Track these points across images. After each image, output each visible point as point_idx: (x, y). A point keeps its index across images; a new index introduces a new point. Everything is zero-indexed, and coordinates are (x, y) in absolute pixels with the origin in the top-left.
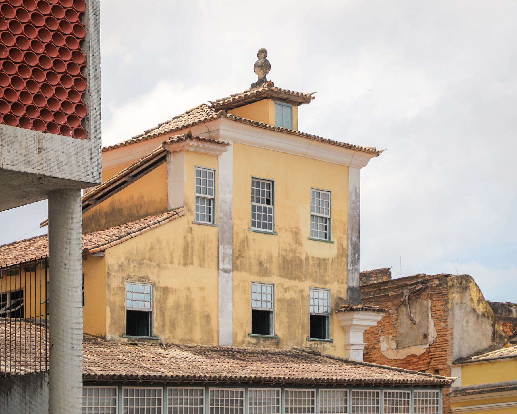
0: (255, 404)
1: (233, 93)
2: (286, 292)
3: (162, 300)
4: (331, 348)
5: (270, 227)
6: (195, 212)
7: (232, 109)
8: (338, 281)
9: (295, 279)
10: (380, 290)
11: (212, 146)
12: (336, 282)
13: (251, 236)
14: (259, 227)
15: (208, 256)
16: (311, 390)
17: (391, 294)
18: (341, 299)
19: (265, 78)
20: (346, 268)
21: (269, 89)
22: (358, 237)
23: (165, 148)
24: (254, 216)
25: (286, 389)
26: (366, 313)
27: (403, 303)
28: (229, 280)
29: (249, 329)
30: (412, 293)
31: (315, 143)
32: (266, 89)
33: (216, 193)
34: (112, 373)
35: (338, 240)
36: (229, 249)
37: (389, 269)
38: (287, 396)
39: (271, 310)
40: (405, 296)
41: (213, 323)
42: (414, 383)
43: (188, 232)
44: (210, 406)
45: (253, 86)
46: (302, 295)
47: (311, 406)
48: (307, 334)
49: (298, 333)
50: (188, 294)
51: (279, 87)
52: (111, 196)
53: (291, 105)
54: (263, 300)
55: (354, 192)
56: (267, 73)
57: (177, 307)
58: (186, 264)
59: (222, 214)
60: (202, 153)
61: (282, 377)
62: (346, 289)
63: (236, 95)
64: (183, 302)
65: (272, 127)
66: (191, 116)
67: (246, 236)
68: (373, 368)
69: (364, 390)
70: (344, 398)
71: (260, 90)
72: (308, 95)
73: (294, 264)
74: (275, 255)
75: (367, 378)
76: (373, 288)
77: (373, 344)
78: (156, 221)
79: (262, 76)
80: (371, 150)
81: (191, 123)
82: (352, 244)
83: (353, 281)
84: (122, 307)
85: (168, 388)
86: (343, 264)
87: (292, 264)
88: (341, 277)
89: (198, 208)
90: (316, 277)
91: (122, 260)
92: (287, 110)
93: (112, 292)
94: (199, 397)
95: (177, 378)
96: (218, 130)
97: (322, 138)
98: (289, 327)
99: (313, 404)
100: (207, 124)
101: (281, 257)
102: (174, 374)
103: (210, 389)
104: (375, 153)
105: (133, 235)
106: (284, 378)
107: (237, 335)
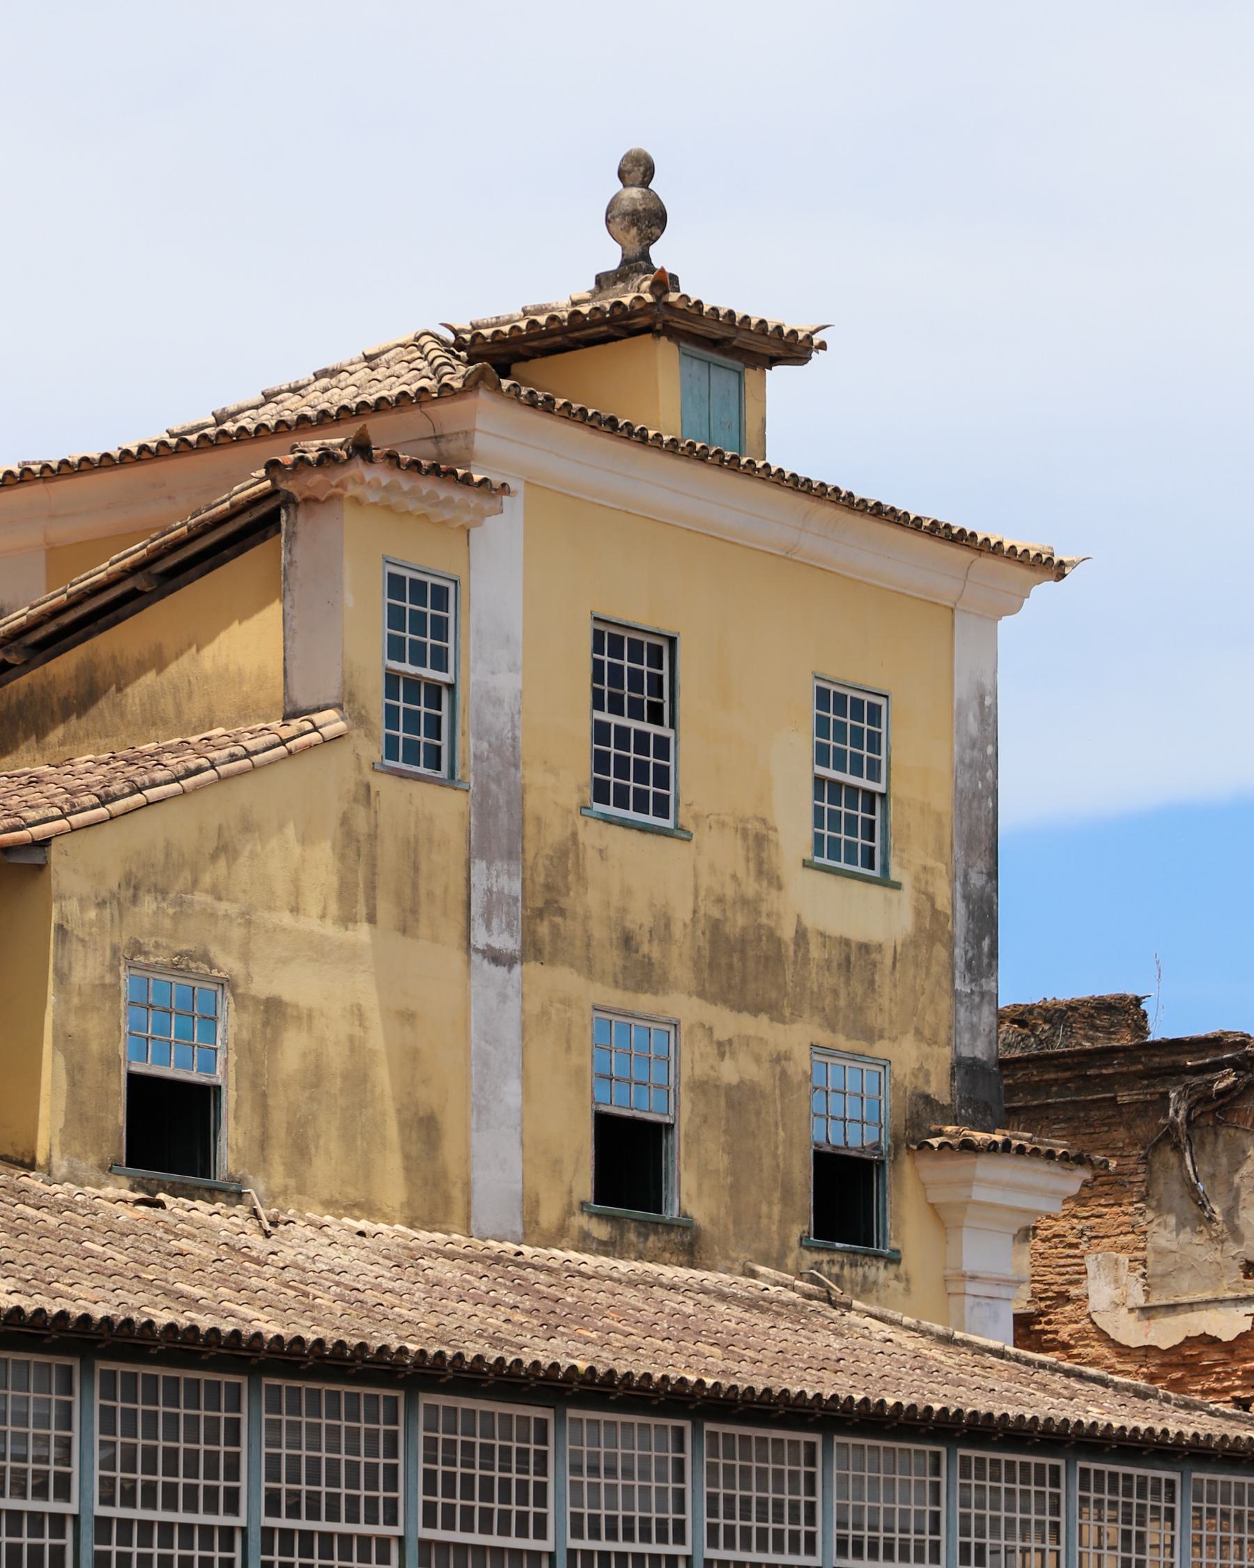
0: (594, 1470)
1: (532, 302)
2: (722, 1055)
3: (259, 1047)
4: (894, 1283)
5: (662, 808)
6: (382, 731)
7: (526, 359)
8: (918, 1032)
9: (756, 1010)
10: (1087, 1078)
11: (444, 491)
12: (910, 1036)
13: (592, 835)
14: (622, 803)
15: (430, 894)
16: (804, 1437)
17: (1124, 1097)
18: (927, 1099)
19: (645, 256)
20: (945, 984)
21: (658, 298)
22: (993, 875)
23: (274, 481)
24: (600, 761)
25: (708, 1427)
26: (1023, 1163)
27: (1169, 1137)
28: (510, 991)
29: (585, 1187)
30: (1198, 1101)
31: (826, 512)
32: (649, 298)
33: (462, 666)
34: (54, 1308)
35: (917, 879)
36: (510, 875)
37: (1138, 1001)
38: (713, 1453)
39: (667, 1120)
40: (1177, 1112)
41: (450, 1150)
42: (1189, 1445)
43: (356, 800)
44: (422, 1466)
45: (603, 281)
46: (784, 1073)
47: (803, 1498)
48: (802, 1226)
49: (769, 1217)
50: (357, 1031)
51: (694, 297)
52: (83, 640)
53: (738, 365)
54: (635, 1077)
55: (975, 704)
56: (654, 240)
57: (315, 1077)
59: (485, 745)
60: (409, 513)
61: (692, 1378)
62: (949, 1066)
63: (540, 310)
64: (336, 1059)
65: (666, 438)
66: (381, 373)
67: (574, 835)
68: (1042, 1376)
69: (1004, 1457)
70: (929, 1479)
71: (627, 300)
72: (801, 336)
73: (750, 953)
74: (682, 914)
75: (1013, 1412)
76: (1059, 1068)
77: (1060, 1279)
78: (238, 750)
79: (636, 249)
80: (1032, 553)
81: (371, 400)
82: (967, 898)
83: (974, 1039)
84: (110, 1062)
85: (267, 1381)
86: (935, 969)
87: (743, 951)
88: (930, 1018)
89: (391, 713)
90: (836, 1010)
91: (113, 883)
92: (723, 381)
93: (76, 1001)
94: (382, 1427)
95: (296, 1348)
96: (468, 434)
97: (850, 495)
98: (735, 1190)
99: (811, 1491)
100: (429, 409)
101: (702, 924)
102: (287, 1333)
103: (425, 1399)
104: (1056, 570)
105: (152, 793)
106: (700, 1383)
107: (537, 1202)
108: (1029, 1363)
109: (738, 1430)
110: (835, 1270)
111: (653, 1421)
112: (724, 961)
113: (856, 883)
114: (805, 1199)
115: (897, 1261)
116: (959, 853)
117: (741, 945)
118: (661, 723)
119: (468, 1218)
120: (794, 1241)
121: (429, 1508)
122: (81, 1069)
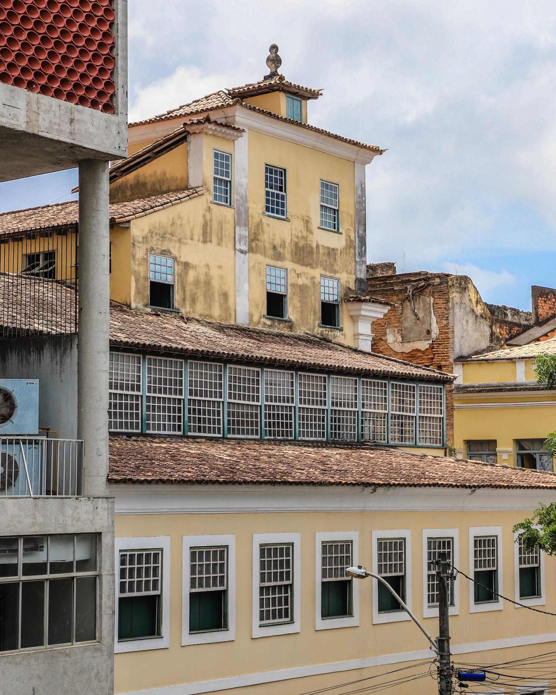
0: (271, 384)
2: (298, 277)
3: (183, 274)
4: (341, 336)
6: (213, 193)
7: (246, 98)
8: (347, 271)
10: (386, 283)
12: (345, 272)
13: (266, 220)
14: (273, 212)
15: (225, 235)
17: (396, 288)
18: (349, 289)
19: (276, 71)
20: (354, 259)
24: (267, 201)
25: (299, 373)
27: (407, 298)
28: (245, 260)
29: (265, 312)
30: (415, 289)
31: (323, 137)
33: (233, 176)
35: (346, 232)
36: (245, 230)
41: (231, 301)
45: (266, 78)
46: (314, 282)
50: (207, 271)
51: (289, 82)
53: (300, 99)
55: (360, 187)
57: (197, 282)
58: (205, 242)
61: (296, 360)
64: (202, 278)
66: (209, 101)
67: (261, 220)
68: (381, 359)
70: (354, 386)
71: (273, 82)
72: (316, 92)
73: (305, 251)
74: (288, 241)
78: (177, 198)
81: (209, 107)
82: (359, 237)
83: (361, 273)
85: (189, 361)
86: (351, 255)
87: (303, 250)
88: (350, 267)
90: (326, 265)
91: (146, 231)
93: (137, 262)
96: (234, 116)
98: (302, 312)
100: (224, 110)
101: (293, 243)
103: (228, 366)
104: (380, 152)
105: (156, 209)
106: (298, 361)
108: (377, 356)
109: (243, 367)
110: (327, 332)
111: (286, 371)
112: (298, 253)
113: (331, 233)
114: (319, 314)
115: (342, 330)
116: (356, 225)
117: (303, 249)
118: (282, 191)
119: (235, 319)
120: (317, 325)
121: (230, 394)
122: (138, 280)
